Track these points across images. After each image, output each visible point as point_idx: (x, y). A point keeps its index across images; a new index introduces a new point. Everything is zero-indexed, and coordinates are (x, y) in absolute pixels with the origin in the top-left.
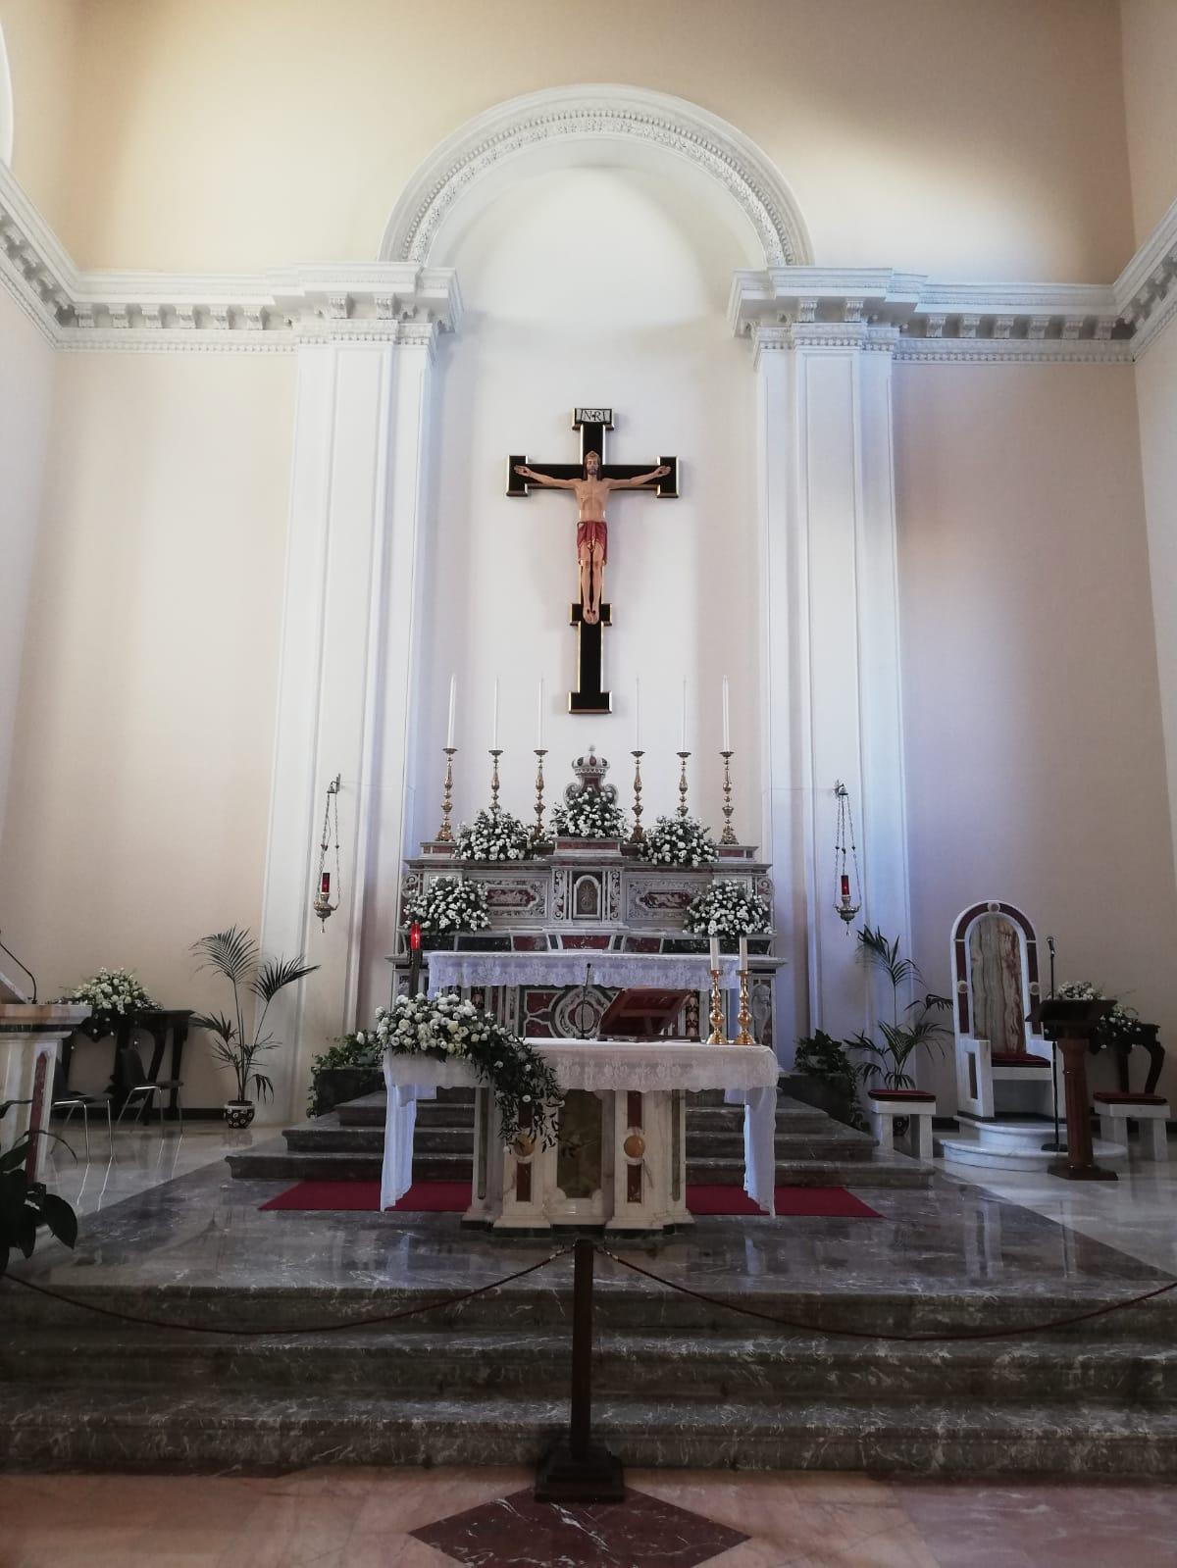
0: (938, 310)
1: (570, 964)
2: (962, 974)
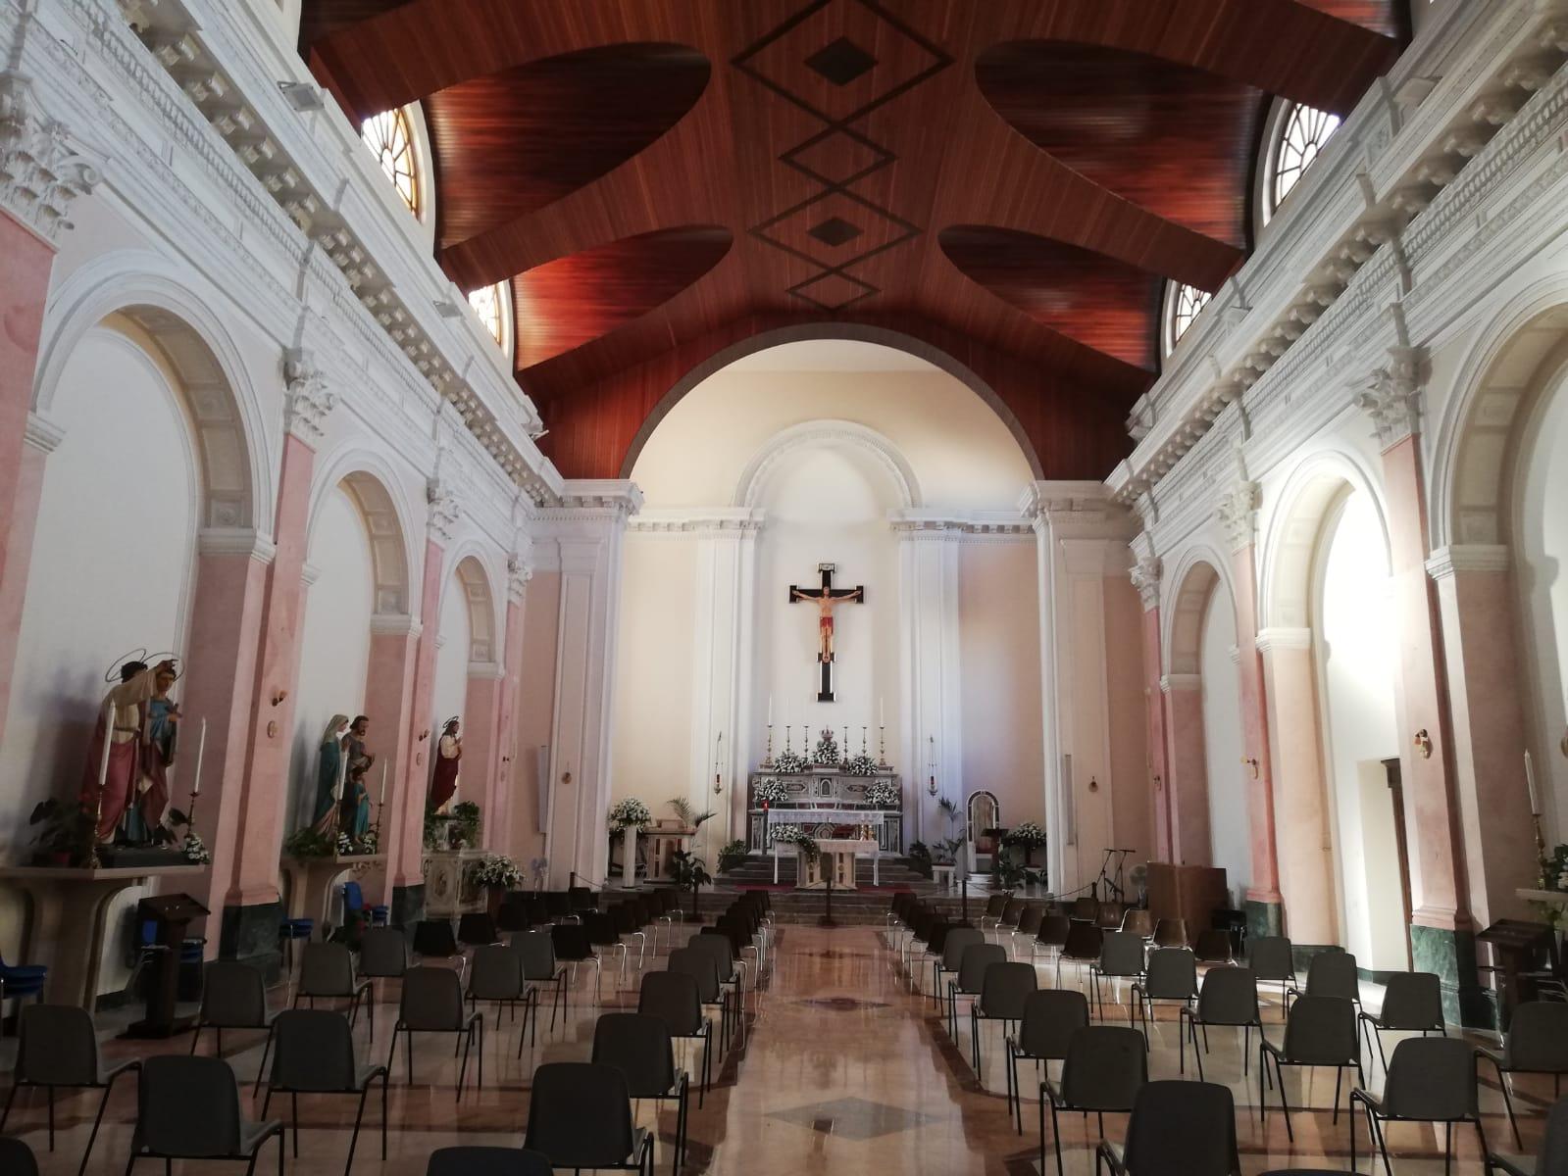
0: (979, 523)
1: (820, 814)
2: (970, 819)
